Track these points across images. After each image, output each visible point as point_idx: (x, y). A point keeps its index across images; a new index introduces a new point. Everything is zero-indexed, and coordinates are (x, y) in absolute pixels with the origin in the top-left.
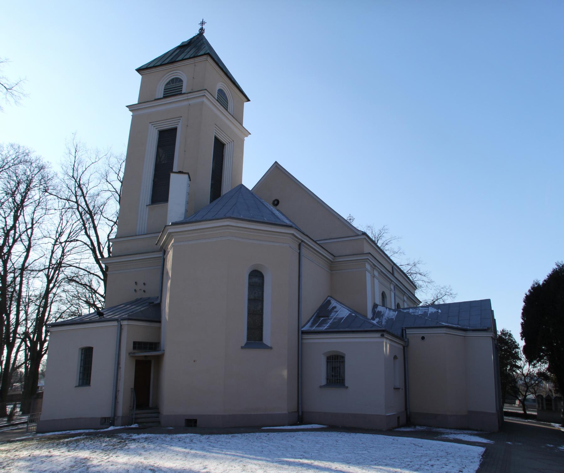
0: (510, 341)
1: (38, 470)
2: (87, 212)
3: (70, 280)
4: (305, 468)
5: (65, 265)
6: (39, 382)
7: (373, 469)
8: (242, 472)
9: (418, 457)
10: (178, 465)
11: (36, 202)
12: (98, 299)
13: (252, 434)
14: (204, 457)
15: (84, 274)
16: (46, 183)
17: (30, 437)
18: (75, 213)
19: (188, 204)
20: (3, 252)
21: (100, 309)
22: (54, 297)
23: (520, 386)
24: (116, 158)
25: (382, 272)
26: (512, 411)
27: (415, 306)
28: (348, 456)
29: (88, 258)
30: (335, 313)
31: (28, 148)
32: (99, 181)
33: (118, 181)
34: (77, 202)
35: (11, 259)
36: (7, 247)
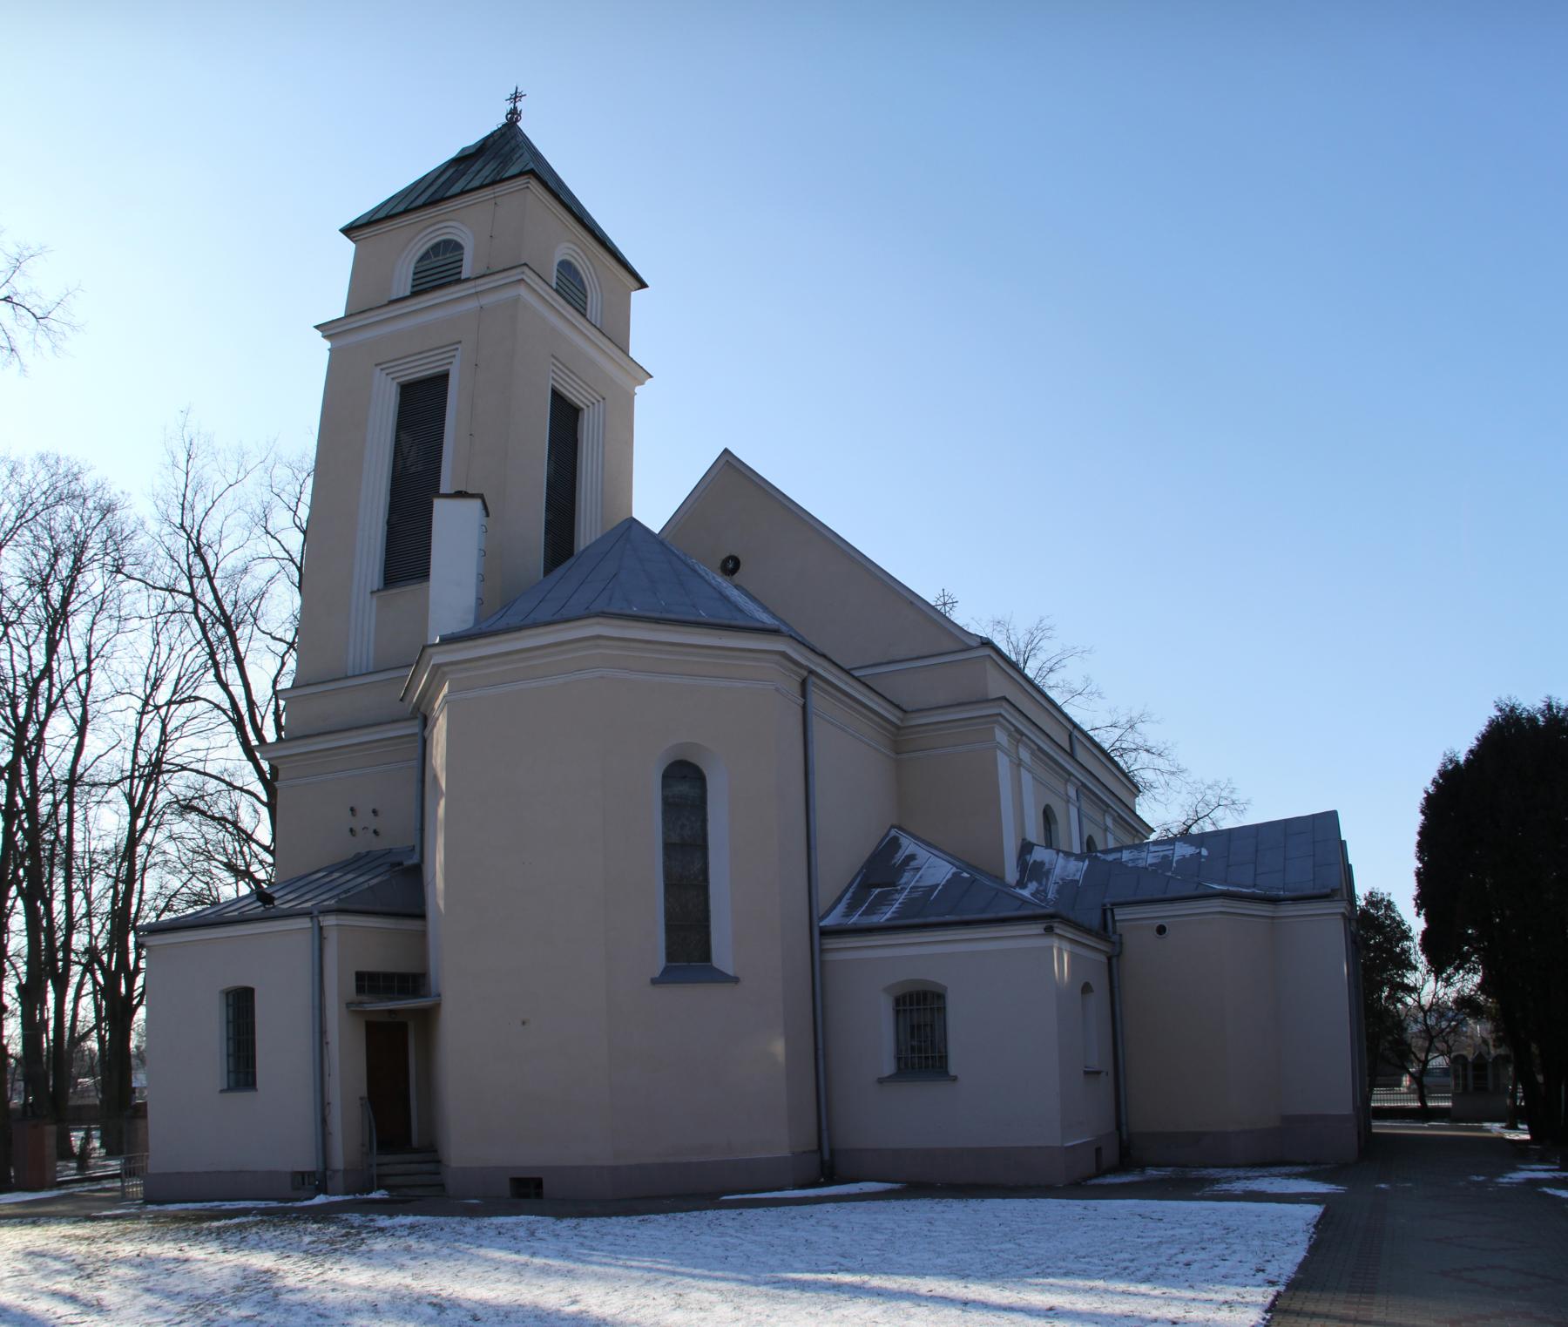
0: (1388, 922)
1: (163, 1290)
2: (218, 620)
3: (186, 807)
4: (847, 1296)
5: (171, 767)
6: (133, 1078)
7: (1031, 1287)
8: (675, 1309)
9: (1150, 1245)
10: (502, 1294)
11: (96, 600)
12: (256, 857)
13: (696, 1213)
14: (569, 1274)
15: (219, 789)
16: (117, 549)
17: (132, 1210)
18: (188, 624)
19: (483, 580)
20: (27, 739)
21: (263, 884)
22: (149, 853)
23: (1413, 1037)
24: (290, 466)
25: (1040, 749)
26: (1392, 1105)
27: (1137, 842)
28: (962, 1260)
29: (225, 744)
30: (912, 873)
31: (78, 460)
32: (246, 534)
33: (297, 529)
34: (192, 595)
35: (46, 755)
36: (35, 723)
